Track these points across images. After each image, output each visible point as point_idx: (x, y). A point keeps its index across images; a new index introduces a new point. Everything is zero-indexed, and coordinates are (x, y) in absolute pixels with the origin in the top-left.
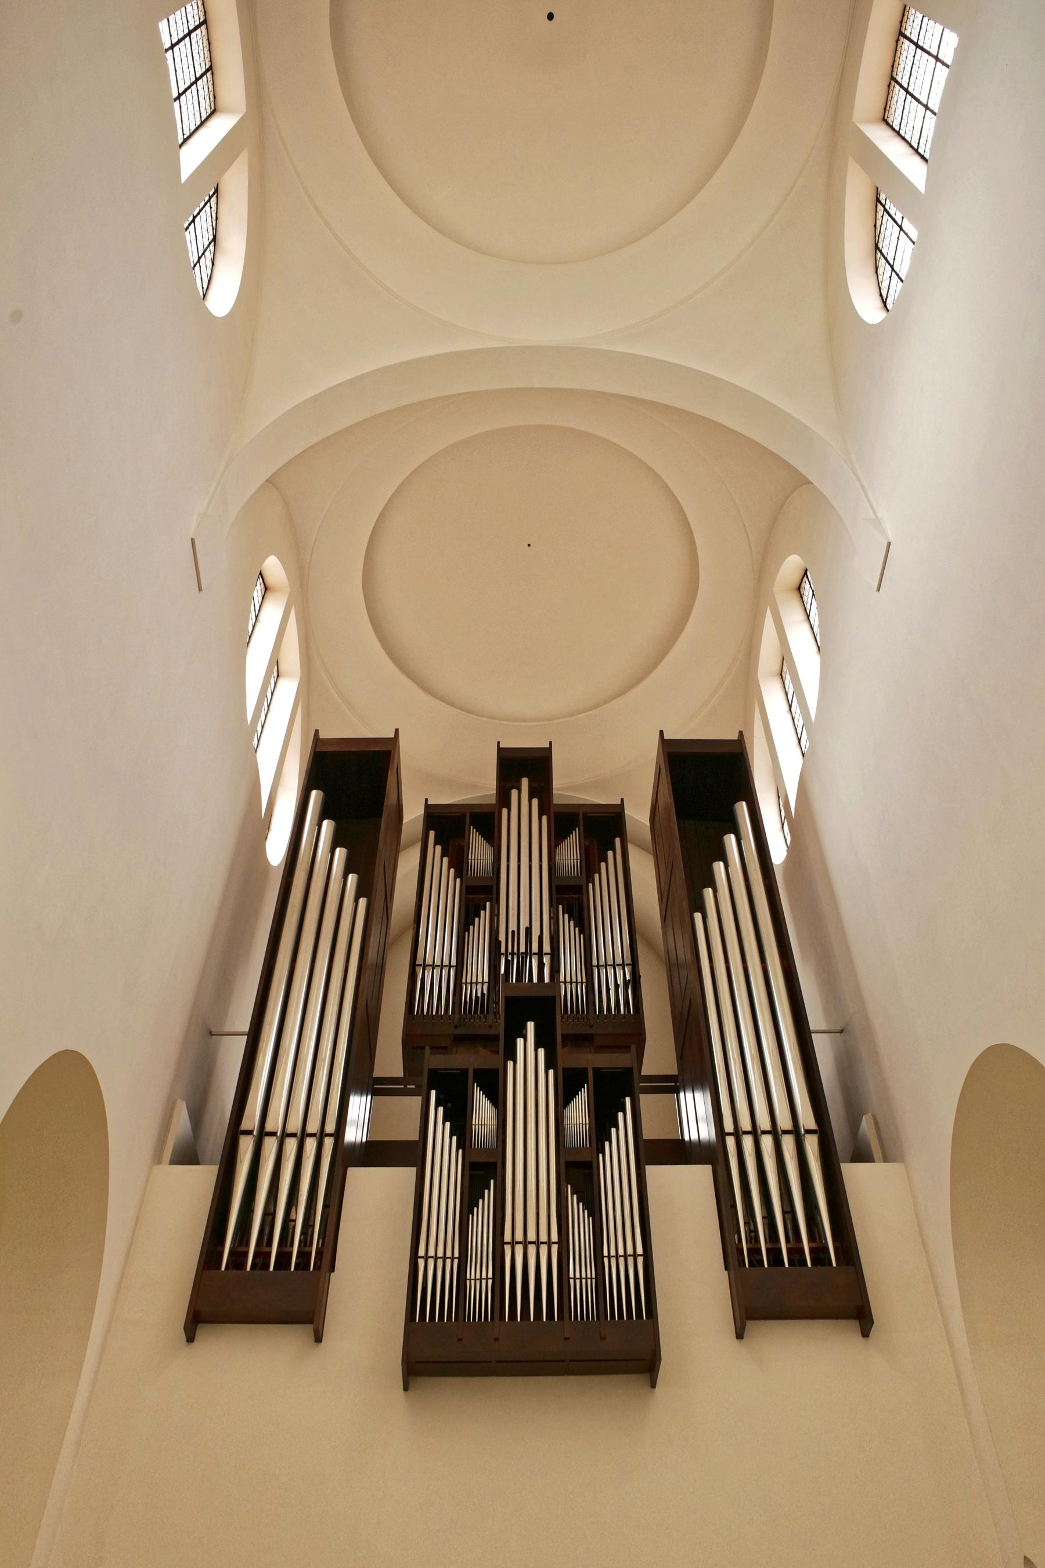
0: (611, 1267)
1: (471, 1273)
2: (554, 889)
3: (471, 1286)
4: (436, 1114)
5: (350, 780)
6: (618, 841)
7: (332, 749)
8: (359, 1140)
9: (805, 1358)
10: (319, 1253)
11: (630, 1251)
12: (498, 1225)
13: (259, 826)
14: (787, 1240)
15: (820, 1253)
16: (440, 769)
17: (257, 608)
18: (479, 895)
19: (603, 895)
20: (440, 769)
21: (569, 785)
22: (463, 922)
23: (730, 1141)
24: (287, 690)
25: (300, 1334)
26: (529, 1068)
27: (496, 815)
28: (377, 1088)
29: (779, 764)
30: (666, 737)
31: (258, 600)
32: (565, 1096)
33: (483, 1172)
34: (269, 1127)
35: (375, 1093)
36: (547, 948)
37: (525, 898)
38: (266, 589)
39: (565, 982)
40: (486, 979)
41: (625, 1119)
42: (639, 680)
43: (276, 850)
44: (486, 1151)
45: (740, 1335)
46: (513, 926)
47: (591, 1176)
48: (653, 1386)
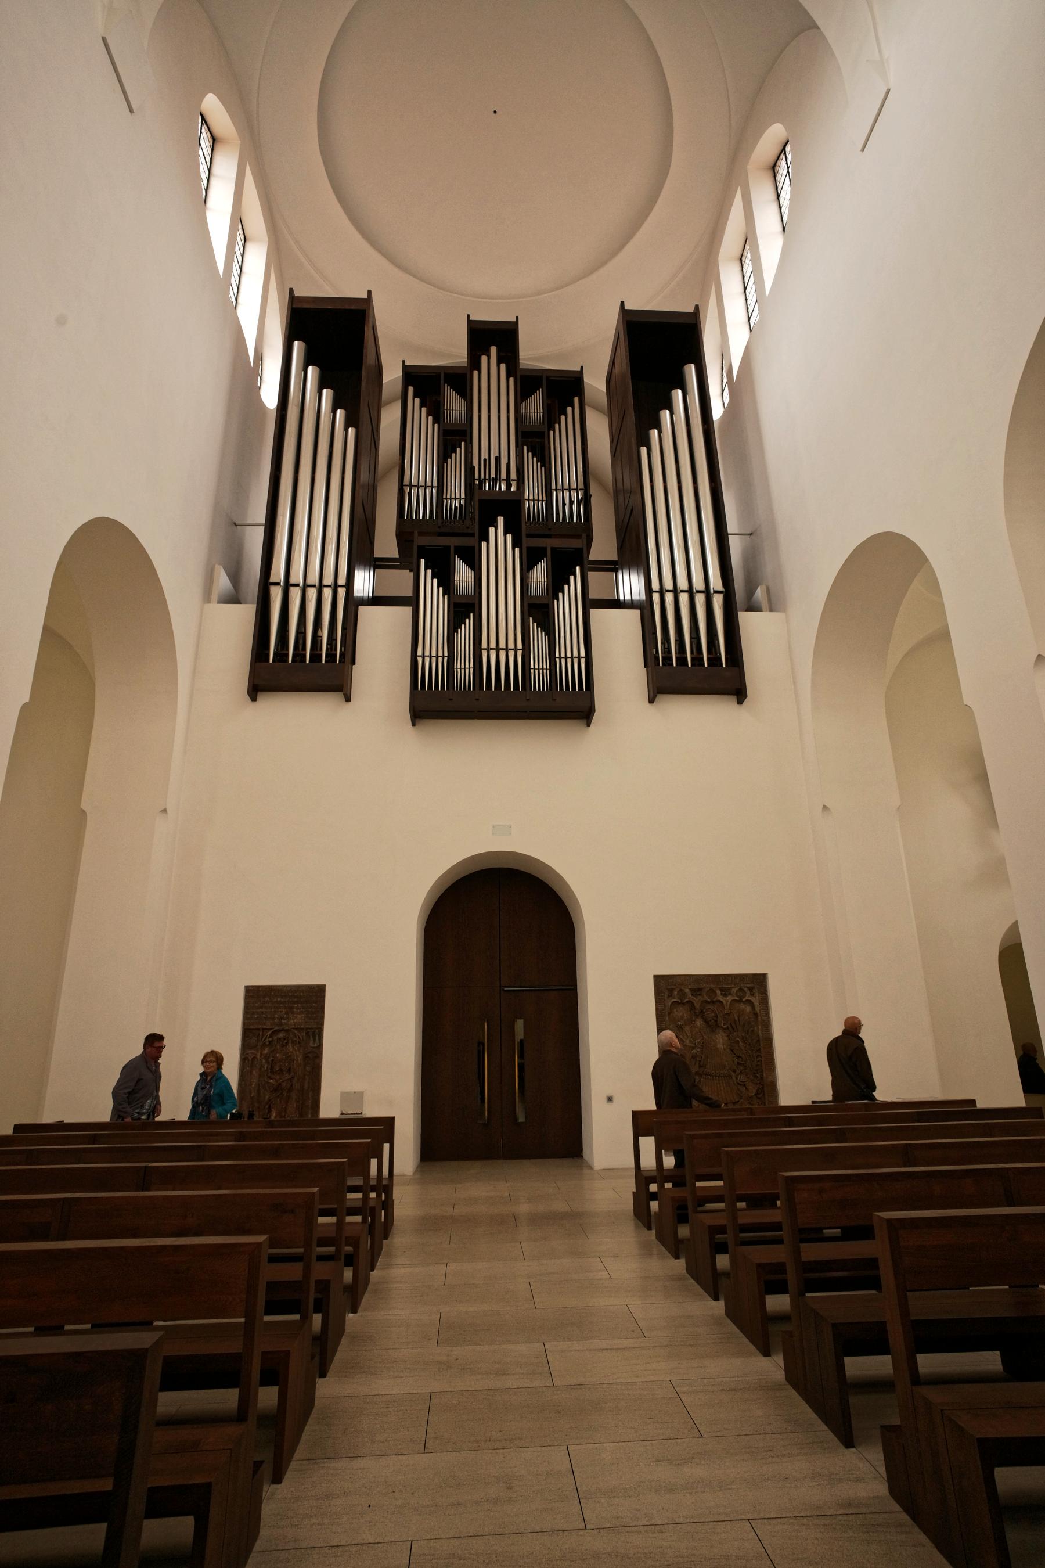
0: (561, 664)
1: (457, 665)
2: (526, 608)
3: (458, 673)
4: (426, 575)
5: (330, 334)
6: (576, 399)
7: (308, 306)
8: (366, 594)
9: (698, 717)
10: (342, 655)
11: (575, 654)
12: (477, 634)
13: (246, 375)
14: (692, 653)
15: (715, 660)
16: (413, 332)
17: (208, 160)
18: (454, 437)
19: (562, 439)
20: (413, 332)
21: (532, 353)
22: (441, 456)
23: (656, 597)
24: (256, 259)
26: (499, 546)
27: (468, 376)
28: (376, 564)
29: (729, 335)
30: (626, 307)
31: (207, 151)
32: (528, 564)
33: (464, 609)
34: (292, 580)
35: (376, 567)
36: (513, 475)
37: (494, 436)
38: (214, 140)
39: (529, 500)
40: (463, 496)
41: (575, 580)
42: (604, 263)
43: (270, 397)
44: (466, 596)
45: (651, 701)
46: (484, 455)
47: (548, 613)
48: (589, 725)
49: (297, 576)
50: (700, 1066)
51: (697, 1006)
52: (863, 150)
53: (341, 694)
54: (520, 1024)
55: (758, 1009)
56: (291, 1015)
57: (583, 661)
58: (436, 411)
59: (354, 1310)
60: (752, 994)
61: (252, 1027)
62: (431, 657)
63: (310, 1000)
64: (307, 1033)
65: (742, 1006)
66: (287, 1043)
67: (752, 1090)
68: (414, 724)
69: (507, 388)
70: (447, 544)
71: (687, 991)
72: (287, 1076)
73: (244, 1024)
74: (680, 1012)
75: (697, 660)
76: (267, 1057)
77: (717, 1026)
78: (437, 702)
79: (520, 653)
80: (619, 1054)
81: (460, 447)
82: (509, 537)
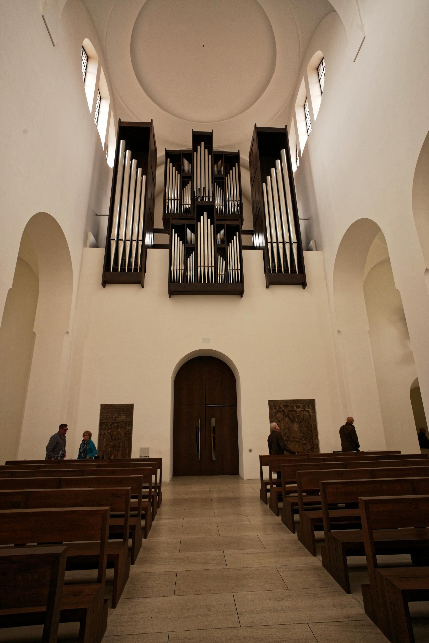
0: (230, 272)
1: (188, 273)
2: (216, 249)
3: (188, 276)
4: (175, 236)
5: (135, 137)
6: (237, 164)
7: (126, 126)
8: (150, 244)
9: (286, 294)
10: (140, 269)
11: (236, 268)
12: (196, 260)
13: (101, 154)
14: (284, 268)
15: (293, 271)
16: (169, 136)
17: (86, 66)
18: (186, 179)
19: (231, 180)
20: (169, 136)
21: (218, 145)
22: (181, 187)
23: (269, 245)
24: (105, 106)
25: (139, 286)
26: (205, 224)
27: (192, 154)
28: (155, 231)
29: (299, 137)
30: (257, 126)
31: (85, 62)
32: (217, 231)
33: (190, 250)
34: (120, 238)
35: (154, 233)
36: (211, 195)
37: (203, 179)
38: (88, 57)
39: (217, 205)
40: (190, 203)
41: (236, 238)
42: (248, 108)
43: (111, 163)
44: (191, 245)
45: (267, 287)
46: (199, 187)
47: (225, 251)
48: (242, 297)
49: (122, 236)
50: (287, 437)
51: (286, 412)
52: (354, 61)
53: (140, 285)
54: (213, 420)
55: (311, 414)
56: (119, 416)
57: (239, 271)
58: (179, 169)
59: (145, 537)
60: (309, 408)
61: (104, 421)
62: (177, 269)
63: (127, 410)
64: (126, 424)
65: (305, 413)
66: (118, 428)
67: (309, 447)
68: (170, 297)
69: (208, 159)
70: (184, 223)
71: (282, 406)
72: (118, 441)
73: (100, 420)
74: (279, 415)
75: (286, 270)
76: (109, 434)
77: (295, 421)
78: (179, 288)
79: (213, 268)
80: (254, 432)
81: (189, 183)
82: (209, 220)
